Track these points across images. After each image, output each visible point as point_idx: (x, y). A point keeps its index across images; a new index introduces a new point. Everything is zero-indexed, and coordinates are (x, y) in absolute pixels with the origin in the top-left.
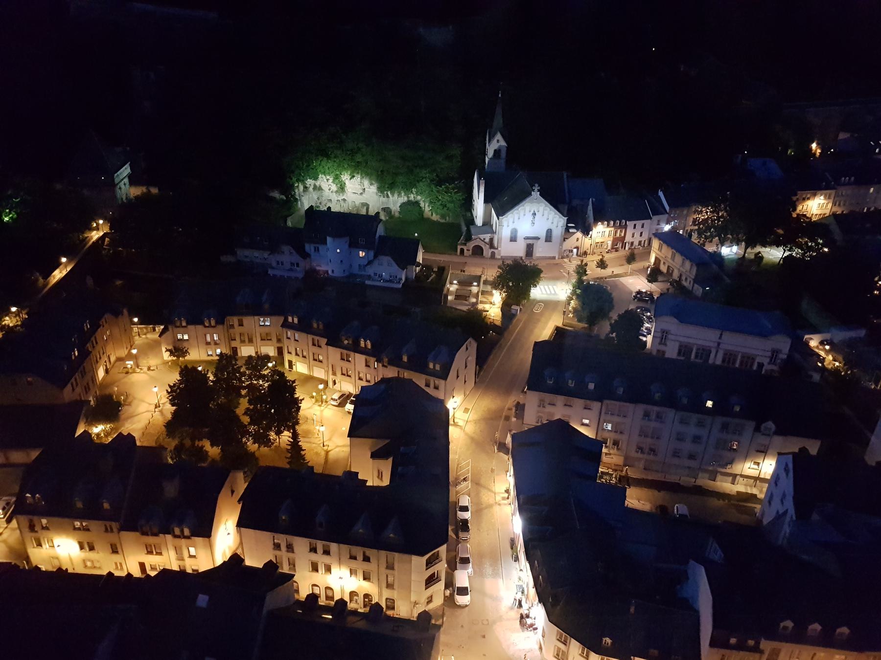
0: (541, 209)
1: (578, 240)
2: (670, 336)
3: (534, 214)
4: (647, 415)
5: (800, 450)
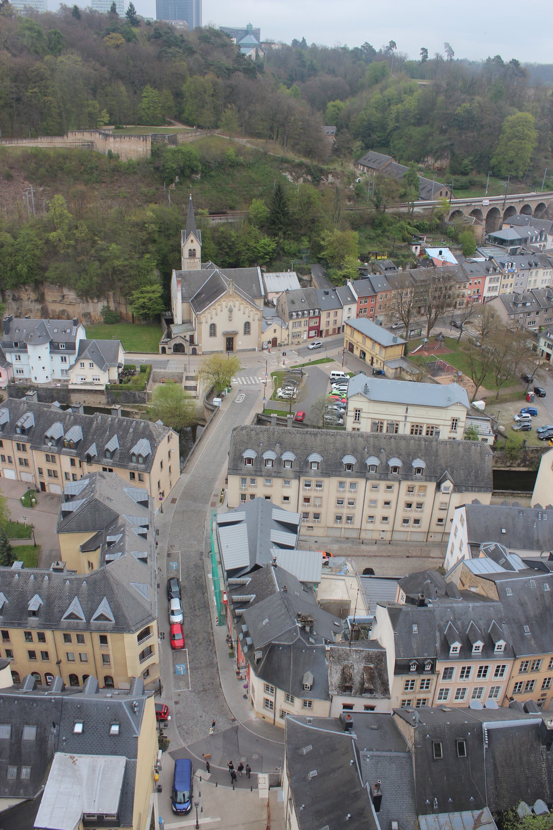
0: (237, 303)
1: (275, 331)
2: (362, 415)
3: (231, 311)
4: (341, 484)
5: (473, 502)
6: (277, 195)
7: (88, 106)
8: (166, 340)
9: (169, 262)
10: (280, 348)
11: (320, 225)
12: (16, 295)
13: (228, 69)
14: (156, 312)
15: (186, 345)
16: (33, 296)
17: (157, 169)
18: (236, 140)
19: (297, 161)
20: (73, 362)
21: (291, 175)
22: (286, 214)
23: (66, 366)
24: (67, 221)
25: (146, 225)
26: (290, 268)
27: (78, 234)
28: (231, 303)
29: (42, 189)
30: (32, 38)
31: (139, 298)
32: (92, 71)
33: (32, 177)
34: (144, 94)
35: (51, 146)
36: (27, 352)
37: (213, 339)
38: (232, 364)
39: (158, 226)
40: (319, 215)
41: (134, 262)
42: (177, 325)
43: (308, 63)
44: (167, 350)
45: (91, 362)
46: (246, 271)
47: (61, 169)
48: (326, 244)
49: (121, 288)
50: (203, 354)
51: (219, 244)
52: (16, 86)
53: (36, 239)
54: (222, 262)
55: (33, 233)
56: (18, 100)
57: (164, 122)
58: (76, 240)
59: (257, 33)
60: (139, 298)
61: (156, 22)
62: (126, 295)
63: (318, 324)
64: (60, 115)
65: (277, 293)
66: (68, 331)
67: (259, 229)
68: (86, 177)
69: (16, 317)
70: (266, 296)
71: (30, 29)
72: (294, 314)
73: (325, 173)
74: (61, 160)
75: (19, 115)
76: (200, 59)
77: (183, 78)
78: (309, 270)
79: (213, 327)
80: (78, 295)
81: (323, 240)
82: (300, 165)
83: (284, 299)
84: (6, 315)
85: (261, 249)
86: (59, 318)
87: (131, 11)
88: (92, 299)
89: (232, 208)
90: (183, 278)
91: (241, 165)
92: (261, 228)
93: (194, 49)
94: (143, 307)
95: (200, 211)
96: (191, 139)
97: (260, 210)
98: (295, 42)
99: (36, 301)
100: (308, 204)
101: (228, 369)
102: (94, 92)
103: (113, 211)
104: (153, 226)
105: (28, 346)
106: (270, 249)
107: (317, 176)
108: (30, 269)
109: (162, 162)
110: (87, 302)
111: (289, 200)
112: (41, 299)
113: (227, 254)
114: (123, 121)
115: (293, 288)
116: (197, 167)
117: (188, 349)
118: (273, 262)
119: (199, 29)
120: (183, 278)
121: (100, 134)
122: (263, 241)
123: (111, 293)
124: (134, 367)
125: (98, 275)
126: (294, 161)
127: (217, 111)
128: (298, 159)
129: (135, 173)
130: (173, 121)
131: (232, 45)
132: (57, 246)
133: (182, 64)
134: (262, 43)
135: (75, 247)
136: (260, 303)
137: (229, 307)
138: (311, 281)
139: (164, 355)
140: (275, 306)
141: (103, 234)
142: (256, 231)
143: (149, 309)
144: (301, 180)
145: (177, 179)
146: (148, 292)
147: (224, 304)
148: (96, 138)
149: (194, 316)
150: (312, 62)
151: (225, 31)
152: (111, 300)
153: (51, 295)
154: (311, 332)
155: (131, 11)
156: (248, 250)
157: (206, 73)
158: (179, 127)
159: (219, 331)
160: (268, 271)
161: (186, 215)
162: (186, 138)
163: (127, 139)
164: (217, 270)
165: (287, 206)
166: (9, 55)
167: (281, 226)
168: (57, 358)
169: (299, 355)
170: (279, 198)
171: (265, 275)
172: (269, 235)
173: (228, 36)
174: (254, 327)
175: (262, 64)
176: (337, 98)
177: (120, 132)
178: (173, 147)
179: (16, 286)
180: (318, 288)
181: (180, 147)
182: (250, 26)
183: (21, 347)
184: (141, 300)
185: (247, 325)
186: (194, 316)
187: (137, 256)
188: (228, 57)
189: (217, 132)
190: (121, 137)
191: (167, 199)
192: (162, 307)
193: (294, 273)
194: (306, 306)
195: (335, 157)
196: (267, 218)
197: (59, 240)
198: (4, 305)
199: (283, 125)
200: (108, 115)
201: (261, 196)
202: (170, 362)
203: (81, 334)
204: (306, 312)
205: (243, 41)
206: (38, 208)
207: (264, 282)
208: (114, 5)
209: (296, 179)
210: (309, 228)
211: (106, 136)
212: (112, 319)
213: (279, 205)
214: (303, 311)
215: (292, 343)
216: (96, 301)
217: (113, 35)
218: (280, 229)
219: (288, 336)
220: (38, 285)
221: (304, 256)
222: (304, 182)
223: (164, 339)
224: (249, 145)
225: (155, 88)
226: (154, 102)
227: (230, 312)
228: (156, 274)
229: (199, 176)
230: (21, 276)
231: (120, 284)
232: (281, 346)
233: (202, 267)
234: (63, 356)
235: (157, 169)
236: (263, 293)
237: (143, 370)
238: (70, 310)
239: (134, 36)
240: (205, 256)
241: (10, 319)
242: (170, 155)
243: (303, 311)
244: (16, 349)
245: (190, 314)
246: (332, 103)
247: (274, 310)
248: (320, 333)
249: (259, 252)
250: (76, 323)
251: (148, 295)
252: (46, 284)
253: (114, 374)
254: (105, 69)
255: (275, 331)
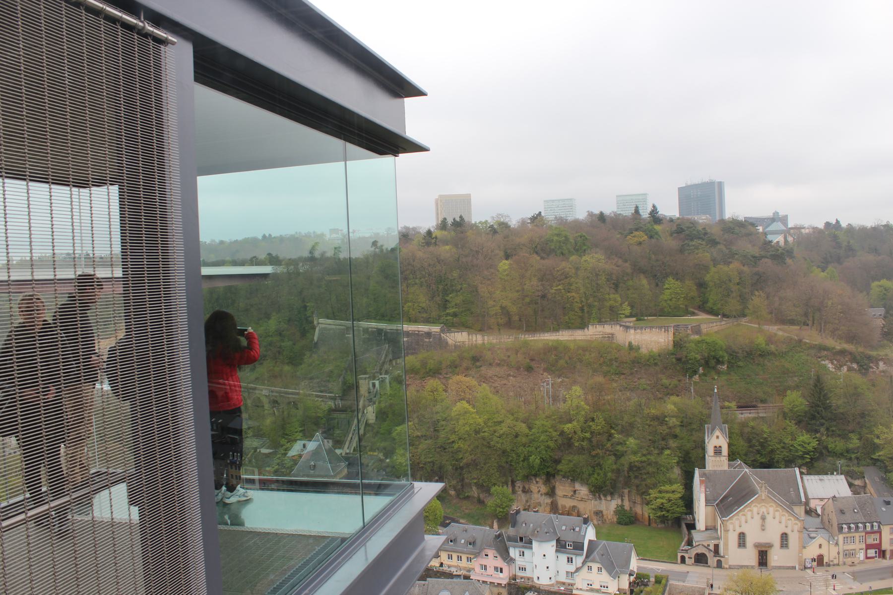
0: (771, 510)
1: (820, 546)
3: (763, 518)
6: (816, 386)
7: (610, 299)
8: (687, 548)
9: (691, 460)
10: (828, 568)
11: (872, 419)
12: (527, 487)
13: (754, 257)
14: (676, 515)
15: (710, 555)
16: (543, 489)
17: (679, 360)
18: (766, 327)
19: (838, 348)
20: (579, 564)
21: (832, 363)
22: (827, 408)
23: (572, 568)
24: (583, 413)
25: (667, 419)
26: (836, 470)
27: (594, 427)
28: (764, 510)
29: (560, 380)
30: (560, 242)
31: (656, 498)
32: (614, 267)
33: (551, 369)
34: (667, 286)
35: (572, 338)
36: (531, 548)
37: (742, 550)
38: (765, 583)
39: (680, 420)
40: (870, 408)
41: (652, 458)
42: (700, 531)
43: (845, 244)
44: (687, 559)
45: (600, 566)
46: (781, 472)
47: (581, 361)
48: (881, 442)
49: (637, 486)
50: (730, 568)
51: (749, 441)
52: (542, 285)
53: (551, 430)
54: (754, 461)
55: (548, 424)
56: (543, 297)
57: (687, 313)
58: (592, 433)
59: (784, 220)
60: (656, 498)
61: (678, 219)
62: (643, 493)
63: (878, 542)
64: (582, 309)
65: (822, 499)
66: (577, 529)
67: (796, 424)
68: (605, 368)
69: (525, 510)
70: (807, 503)
71: (558, 235)
72: (845, 526)
73: (876, 361)
74: (580, 352)
75: (543, 310)
76: (724, 248)
77: (706, 268)
78: (862, 473)
79: (742, 537)
80: (591, 491)
81: (878, 437)
82: (842, 352)
83: (831, 507)
84: (515, 507)
85: (799, 448)
86: (568, 514)
87: (654, 211)
88: (605, 496)
89: (763, 401)
90: (707, 479)
91: (773, 354)
92: (799, 423)
93: (718, 240)
94: (661, 508)
95: (727, 404)
96: (716, 329)
97: (796, 403)
98: (828, 224)
99: (547, 494)
100: (855, 394)
101: (761, 590)
102: (616, 286)
103: (632, 403)
104: (674, 419)
105: (534, 542)
106: (810, 448)
107: (864, 364)
108: (543, 460)
109: (685, 353)
110: (600, 499)
111: (831, 392)
112: (551, 493)
113: (758, 452)
114: (644, 312)
115: (842, 495)
116: (723, 357)
117: (712, 560)
118: (815, 463)
119: (722, 221)
120: (707, 478)
121: (621, 326)
122: (801, 438)
123: (626, 491)
124: (647, 577)
125: (613, 471)
126: (834, 348)
127: (743, 299)
128: (839, 346)
129: (656, 364)
130: (696, 311)
131: (758, 233)
132: (571, 438)
133: (705, 255)
134: (791, 228)
135: (590, 440)
136: (800, 510)
137: (761, 513)
138: (865, 487)
139: (683, 565)
140: (819, 515)
141: (620, 427)
142: (792, 426)
143: (668, 511)
144: (845, 368)
145: (701, 370)
146: (667, 492)
147: (755, 510)
148: (616, 330)
149: (719, 522)
150: (849, 242)
151: (750, 221)
152: (626, 498)
153: (562, 489)
154: (869, 551)
155: (654, 211)
156: (783, 448)
157: (731, 262)
158: (703, 316)
159: (750, 541)
160: (809, 474)
161: (711, 408)
162: (710, 328)
163: (648, 330)
164: (747, 470)
165: (828, 399)
166: (538, 258)
167: (823, 421)
168: (563, 558)
169: (855, 579)
170: (819, 391)
171: (805, 477)
172: (808, 431)
173: (753, 225)
174: (794, 540)
175: (792, 249)
176: (883, 278)
177: (641, 323)
178: (697, 337)
179: (527, 478)
180: (875, 496)
181: (704, 337)
182: (776, 213)
183: (525, 542)
184: (659, 501)
185: (784, 537)
186: (719, 522)
187: (656, 452)
188: (754, 245)
189: (743, 321)
190: (641, 328)
191: (690, 391)
192: (682, 509)
193: (843, 477)
194: (860, 518)
195: (885, 342)
196: (806, 412)
197: (575, 432)
198: (513, 497)
199: (819, 310)
200: (629, 308)
201: (797, 387)
202: (690, 574)
203: (590, 534)
204: (860, 525)
205: (769, 229)
206: (555, 399)
207: (804, 487)
208: (637, 207)
209: (839, 368)
210: (859, 423)
211: (627, 328)
212: (627, 519)
213: (819, 398)
214: (856, 524)
215: (844, 564)
216: (609, 498)
217: (637, 233)
218: (822, 425)
219: (839, 553)
220: (549, 477)
221: (853, 456)
222: (848, 370)
223: (683, 546)
224: (780, 333)
225: (677, 280)
226: (677, 293)
227: (762, 520)
228: (677, 472)
229: (725, 367)
230: (533, 467)
231: (637, 482)
232: (829, 565)
233: (729, 466)
234: (570, 556)
235: (679, 360)
236: (803, 499)
237: (658, 581)
238: (581, 506)
239: (657, 233)
240: (733, 454)
241: (518, 512)
242: (693, 345)
243: (856, 524)
244: (521, 544)
245: (715, 520)
246: (876, 283)
247: (818, 520)
248: (882, 554)
249: (797, 451)
250: (586, 521)
251: (667, 495)
252: (558, 477)
253: (625, 582)
254: (627, 264)
255: (820, 546)
